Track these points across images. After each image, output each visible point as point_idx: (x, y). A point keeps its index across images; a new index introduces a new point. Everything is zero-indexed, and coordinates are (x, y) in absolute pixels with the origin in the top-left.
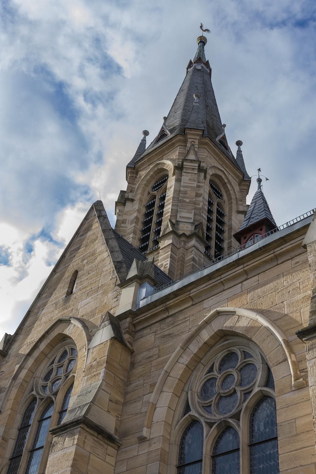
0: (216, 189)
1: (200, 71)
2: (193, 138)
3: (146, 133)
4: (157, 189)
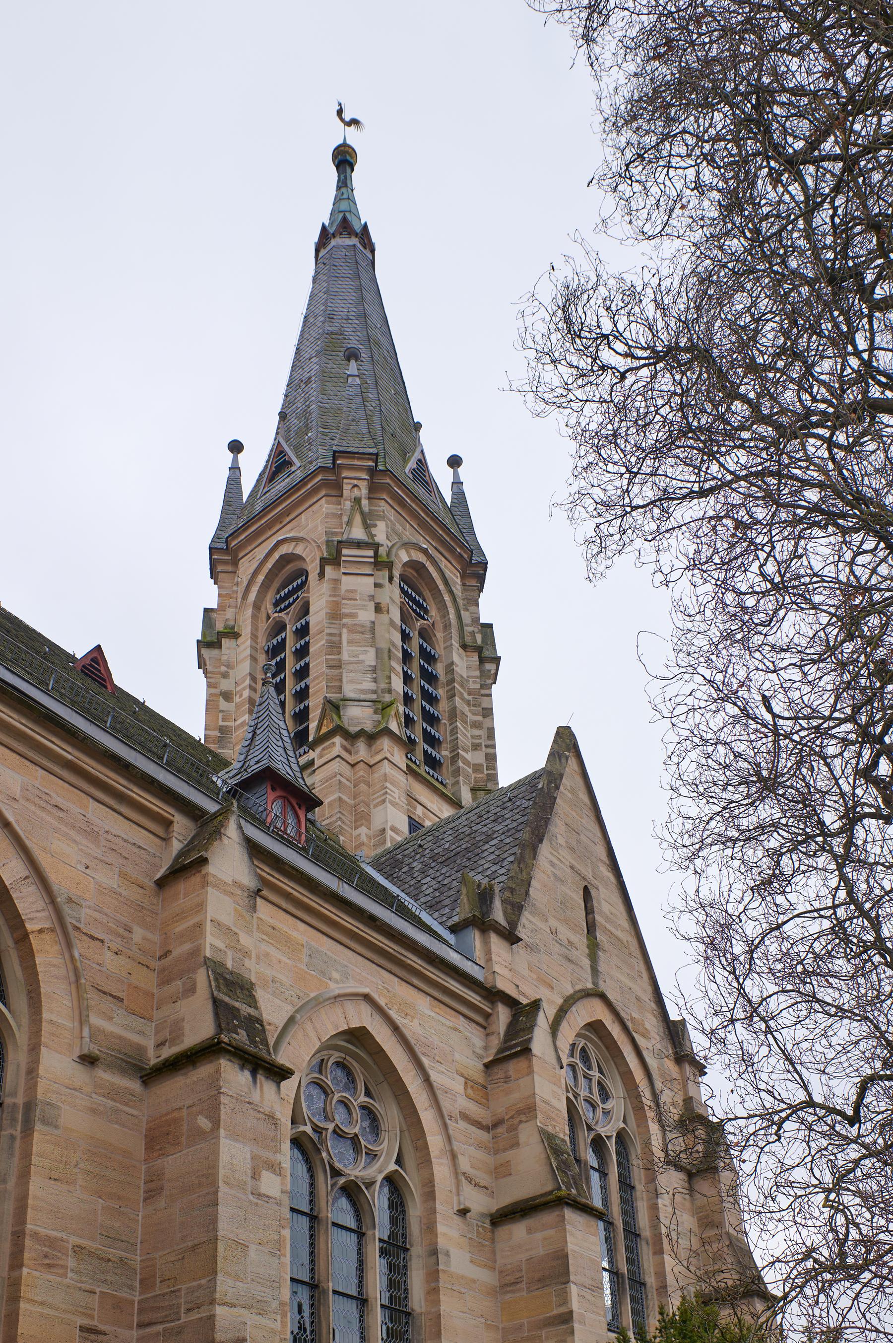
0: (416, 585)
1: (345, 243)
2: (356, 486)
3: (236, 447)
4: (286, 608)
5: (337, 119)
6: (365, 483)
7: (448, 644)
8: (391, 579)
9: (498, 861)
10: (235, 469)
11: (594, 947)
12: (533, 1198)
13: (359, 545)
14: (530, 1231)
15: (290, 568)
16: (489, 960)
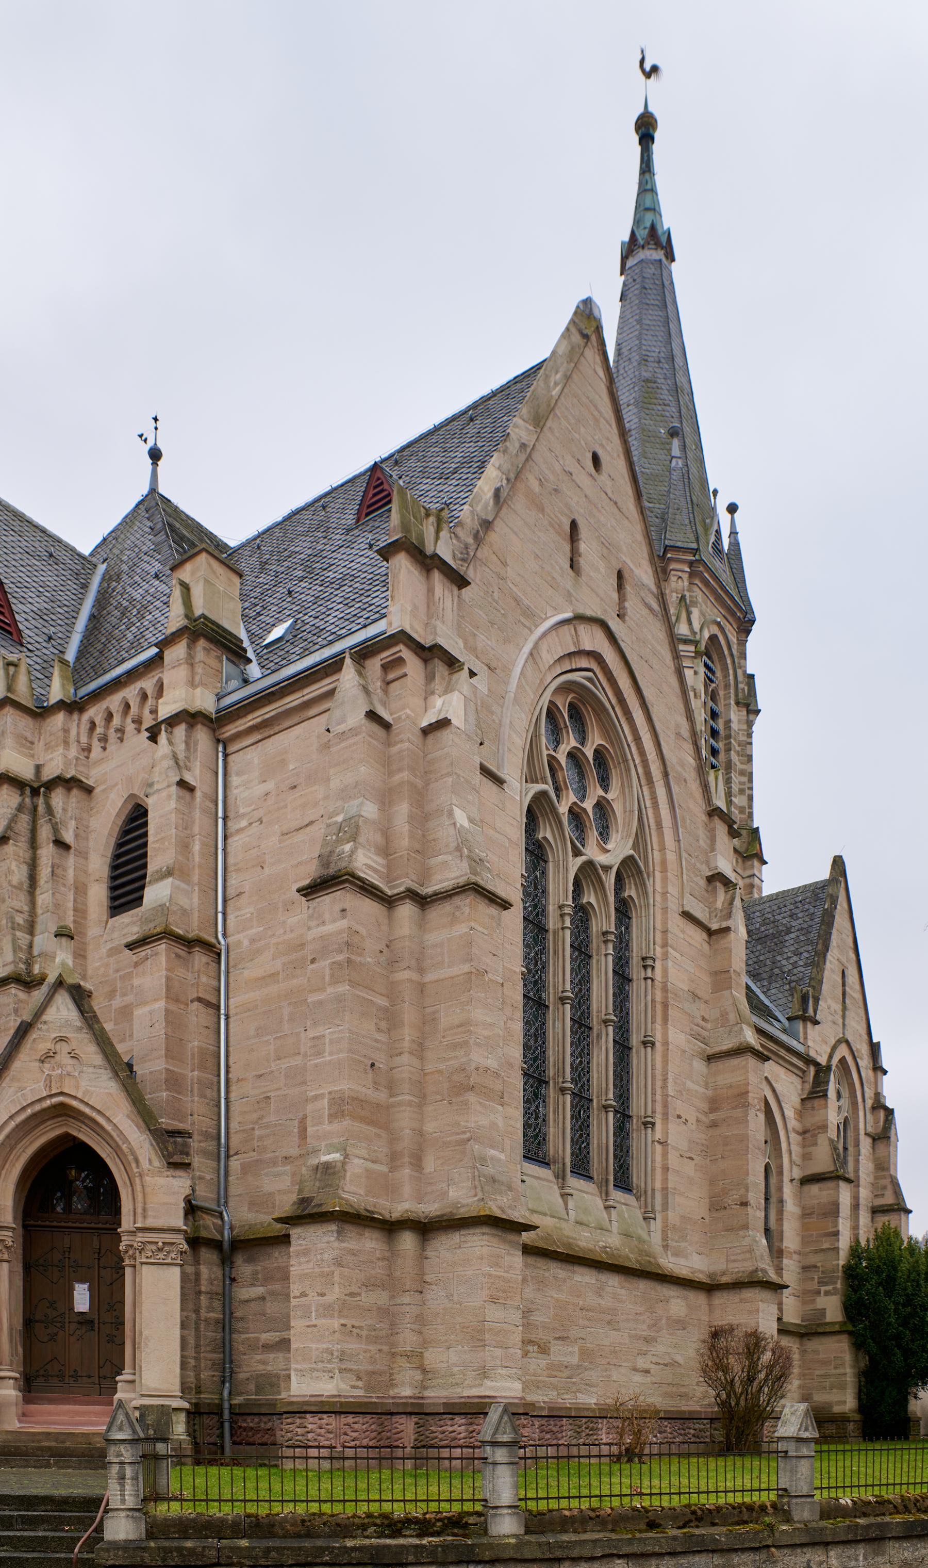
7: (727, 702)
9: (797, 953)
11: (844, 1008)
12: (824, 1173)
14: (820, 1190)
16: (806, 1038)
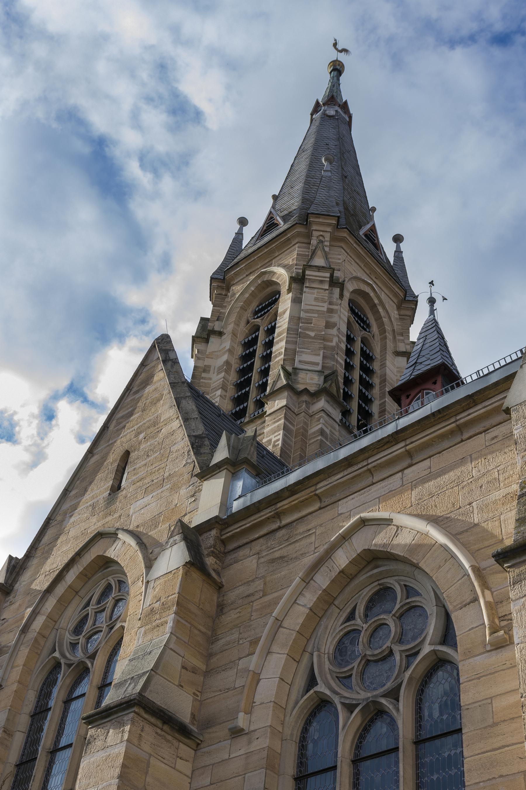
1: (333, 118)
2: (322, 231)
3: (243, 222)
5: (333, 48)
6: (329, 234)
8: (341, 296)
10: (239, 235)
13: (319, 268)
15: (269, 290)
